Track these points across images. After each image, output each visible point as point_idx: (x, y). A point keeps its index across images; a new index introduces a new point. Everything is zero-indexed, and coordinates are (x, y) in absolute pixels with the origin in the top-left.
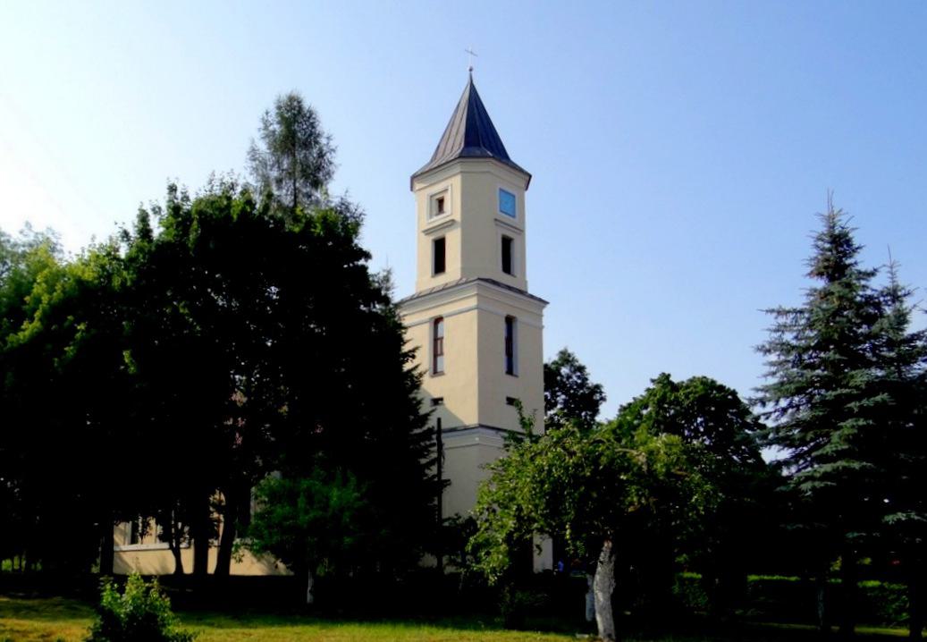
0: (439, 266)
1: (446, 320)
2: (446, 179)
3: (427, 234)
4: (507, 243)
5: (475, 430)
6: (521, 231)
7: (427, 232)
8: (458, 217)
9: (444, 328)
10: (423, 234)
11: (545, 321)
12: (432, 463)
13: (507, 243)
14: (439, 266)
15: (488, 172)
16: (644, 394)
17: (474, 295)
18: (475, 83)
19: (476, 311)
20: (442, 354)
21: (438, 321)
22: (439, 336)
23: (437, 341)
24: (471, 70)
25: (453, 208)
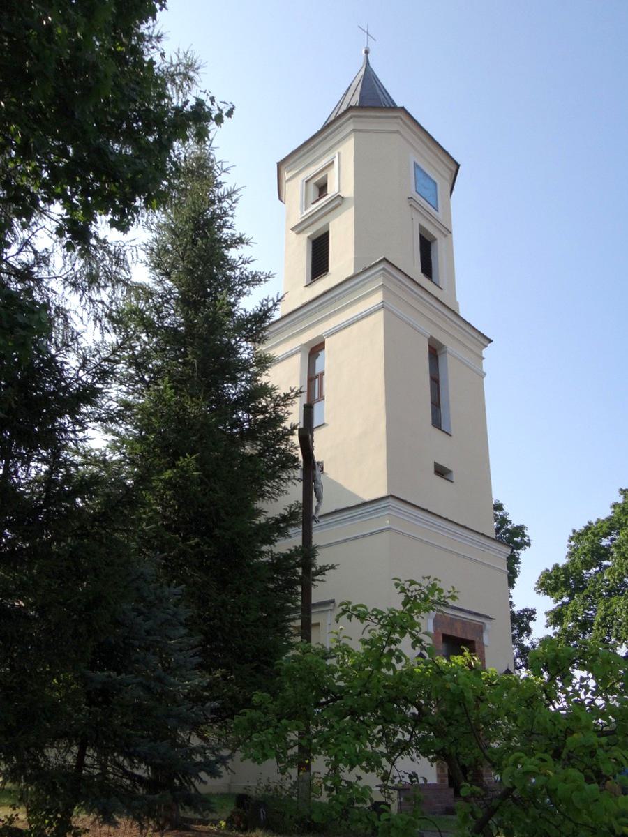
0: (319, 263)
1: (328, 342)
2: (329, 150)
3: (297, 233)
4: (426, 246)
5: (384, 504)
6: (447, 232)
7: (298, 229)
8: (348, 191)
9: (326, 362)
10: (293, 233)
11: (486, 366)
12: (286, 520)
13: (426, 246)
14: (319, 263)
15: (397, 132)
16: (124, 822)
17: (378, 289)
18: (372, 65)
19: (381, 314)
20: (322, 398)
21: (315, 350)
22: (318, 371)
23: (313, 378)
24: (367, 52)
25: (342, 181)
